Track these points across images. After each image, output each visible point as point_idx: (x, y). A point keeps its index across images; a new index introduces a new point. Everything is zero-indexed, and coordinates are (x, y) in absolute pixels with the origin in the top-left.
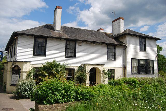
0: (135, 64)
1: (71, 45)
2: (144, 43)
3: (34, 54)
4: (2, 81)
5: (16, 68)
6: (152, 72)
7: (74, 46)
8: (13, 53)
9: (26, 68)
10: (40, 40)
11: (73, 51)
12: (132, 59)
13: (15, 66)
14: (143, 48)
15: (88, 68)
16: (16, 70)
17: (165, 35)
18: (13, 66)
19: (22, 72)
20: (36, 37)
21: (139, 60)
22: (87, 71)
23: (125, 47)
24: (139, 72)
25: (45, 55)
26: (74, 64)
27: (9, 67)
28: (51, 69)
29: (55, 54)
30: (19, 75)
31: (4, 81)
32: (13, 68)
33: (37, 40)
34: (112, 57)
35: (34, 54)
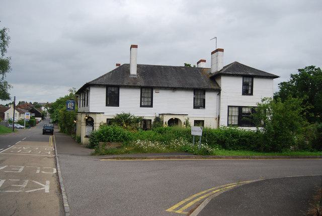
0: (235, 112)
1: (248, 80)
2: (250, 84)
3: (107, 105)
4: (75, 133)
5: (90, 120)
6: (250, 92)
7: (150, 96)
8: (86, 103)
9: (100, 120)
10: (113, 90)
11: (150, 100)
12: (229, 106)
13: (89, 117)
14: (247, 90)
15: (166, 119)
16: (89, 122)
17: (3, 136)
18: (87, 118)
19: (96, 123)
20: (107, 87)
21: (240, 108)
22: (164, 122)
23: (218, 91)
24: (241, 123)
25: (118, 105)
26: (149, 114)
27: (82, 118)
28: (123, 120)
29: (130, 103)
30: (93, 126)
31: (77, 132)
32: (87, 120)
33: (110, 89)
34: (200, 104)
35: (107, 105)
